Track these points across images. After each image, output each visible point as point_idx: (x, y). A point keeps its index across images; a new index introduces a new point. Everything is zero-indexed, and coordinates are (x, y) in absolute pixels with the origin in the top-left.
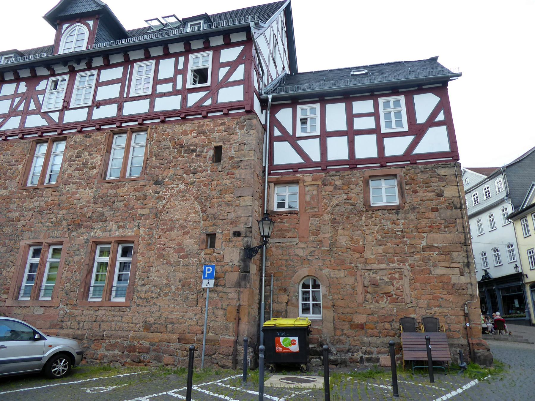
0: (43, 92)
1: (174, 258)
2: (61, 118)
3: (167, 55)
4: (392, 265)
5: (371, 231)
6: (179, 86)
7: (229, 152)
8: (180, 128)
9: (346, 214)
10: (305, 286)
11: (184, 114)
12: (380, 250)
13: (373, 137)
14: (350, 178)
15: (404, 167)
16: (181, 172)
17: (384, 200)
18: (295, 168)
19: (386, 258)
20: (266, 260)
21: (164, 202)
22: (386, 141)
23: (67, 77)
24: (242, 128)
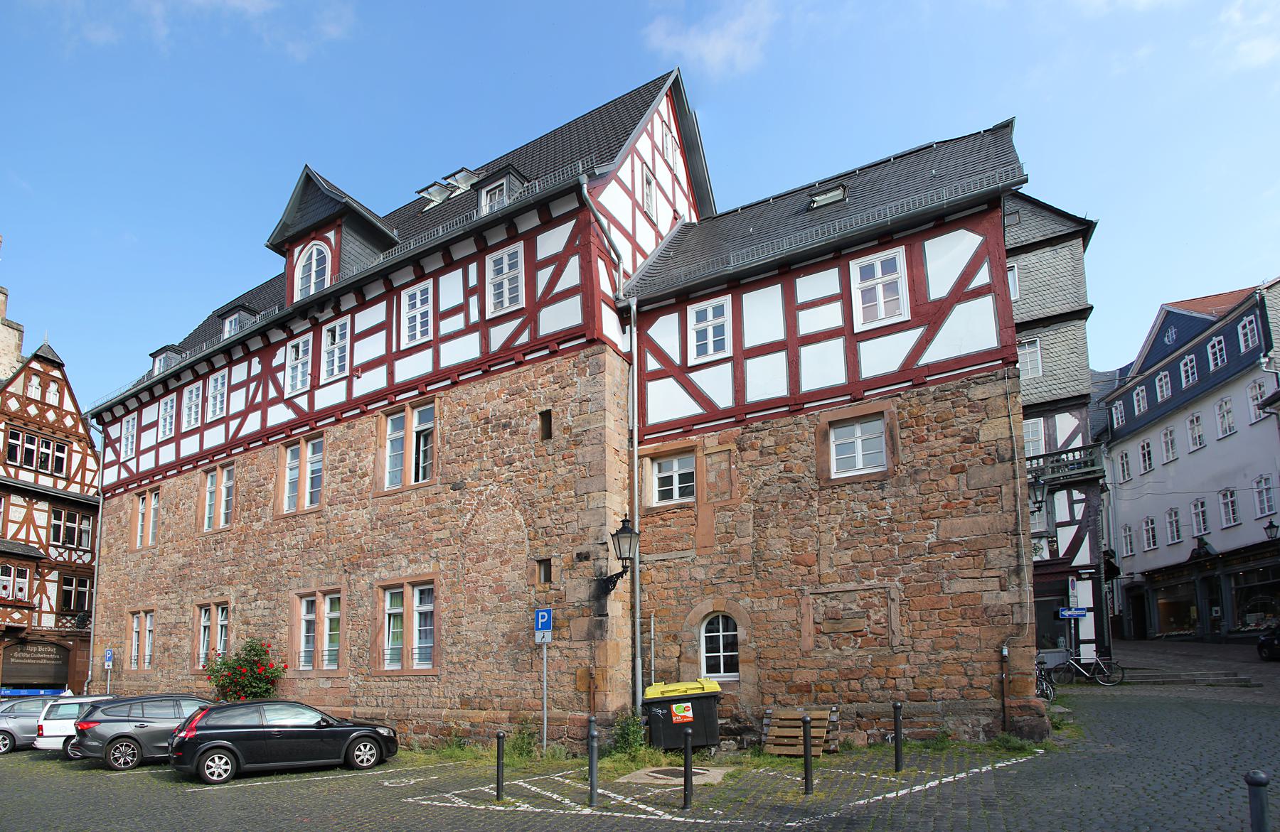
0: (282, 367)
1: (491, 601)
3: (450, 266)
4: (867, 583)
5: (829, 526)
8: (482, 390)
9: (782, 499)
10: (712, 627)
11: (486, 365)
12: (846, 557)
13: (838, 344)
16: (489, 465)
17: (860, 464)
18: (686, 426)
19: (857, 569)
20: (642, 590)
21: (469, 516)
22: (864, 347)
23: (310, 336)
24: (582, 373)
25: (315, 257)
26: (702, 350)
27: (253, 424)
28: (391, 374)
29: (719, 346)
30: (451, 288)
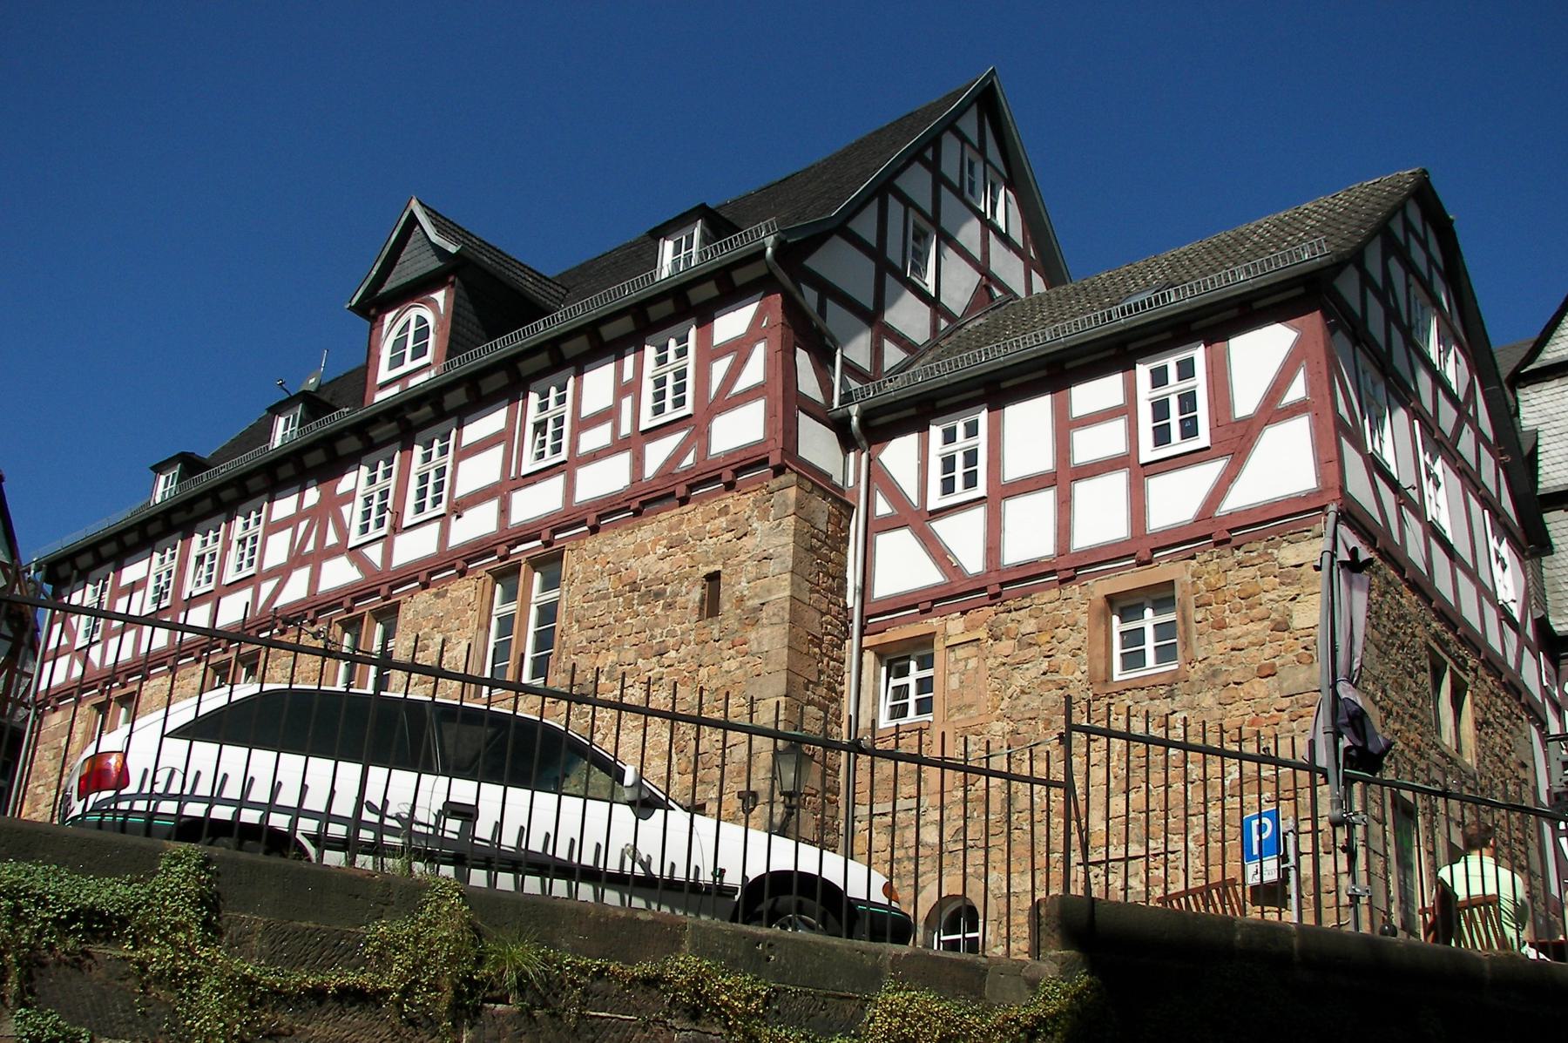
0: (350, 497)
2: (388, 554)
6: (626, 429)
7: (737, 586)
8: (631, 538)
11: (640, 502)
13: (1120, 479)
14: (1056, 609)
15: (1193, 558)
24: (764, 516)
25: (412, 328)
26: (948, 487)
27: (296, 589)
28: (504, 511)
29: (970, 480)
30: (598, 385)
